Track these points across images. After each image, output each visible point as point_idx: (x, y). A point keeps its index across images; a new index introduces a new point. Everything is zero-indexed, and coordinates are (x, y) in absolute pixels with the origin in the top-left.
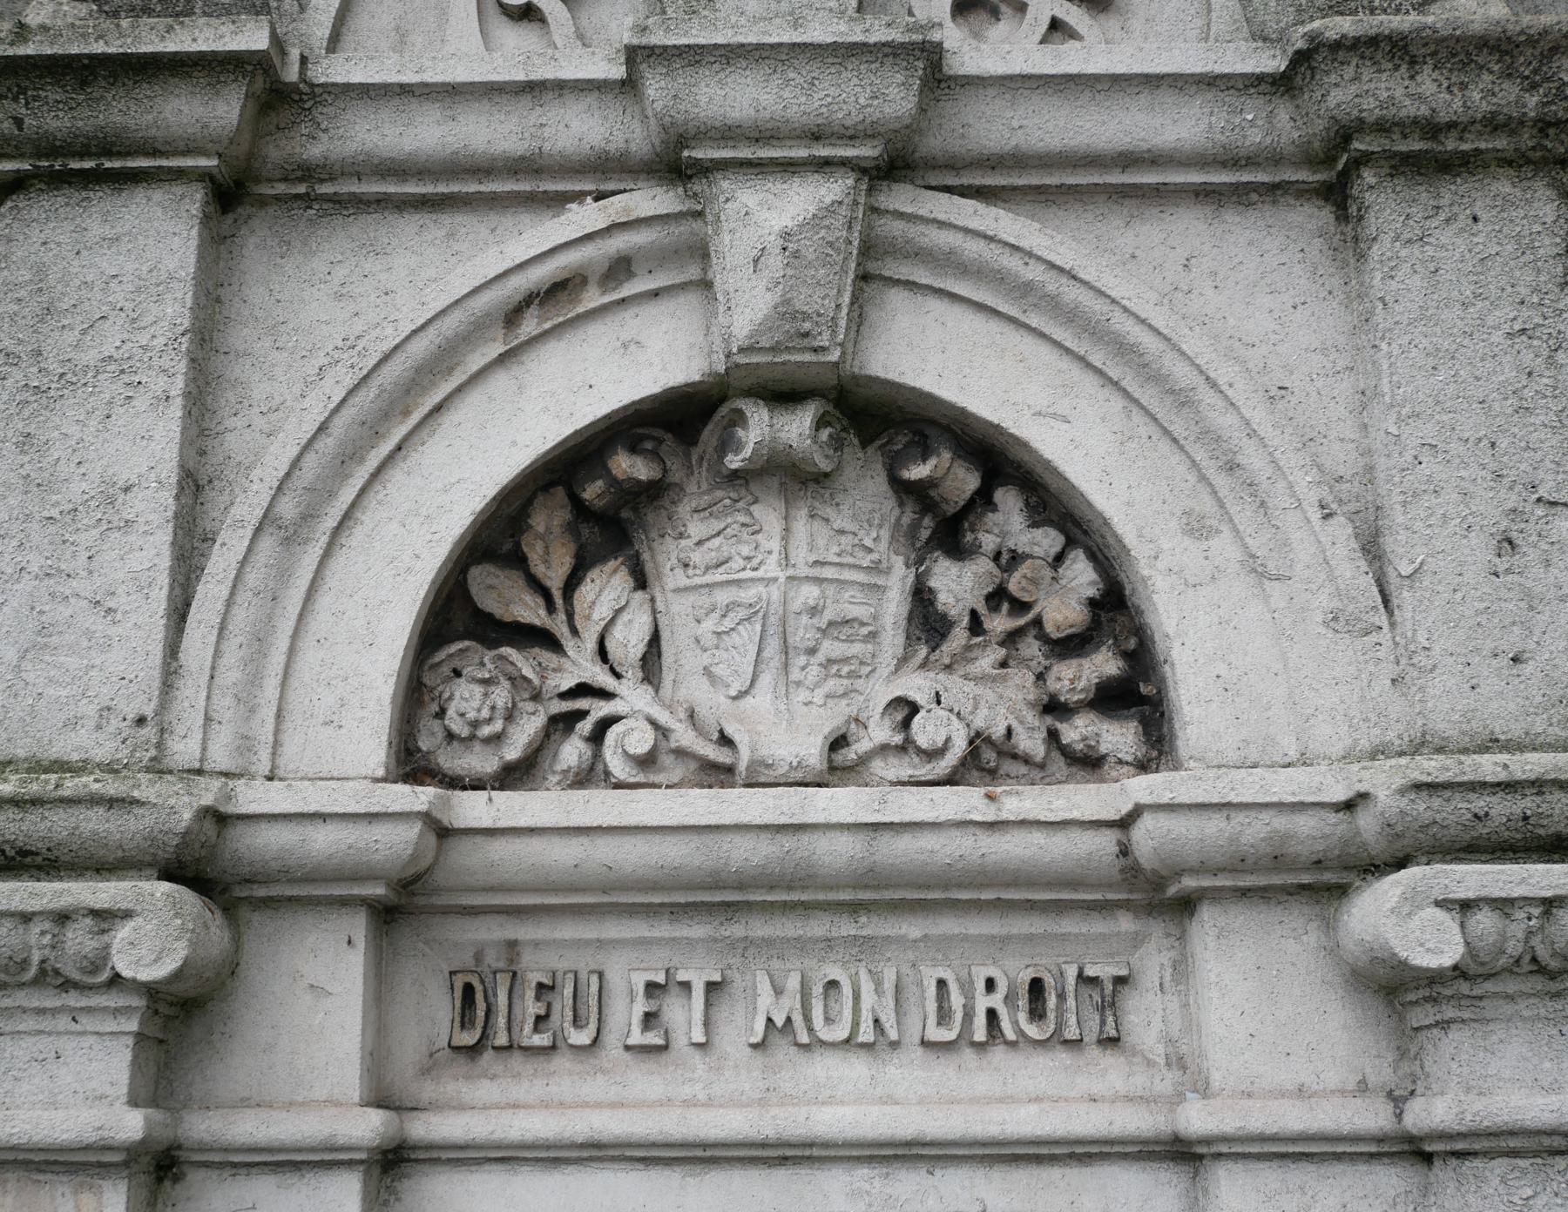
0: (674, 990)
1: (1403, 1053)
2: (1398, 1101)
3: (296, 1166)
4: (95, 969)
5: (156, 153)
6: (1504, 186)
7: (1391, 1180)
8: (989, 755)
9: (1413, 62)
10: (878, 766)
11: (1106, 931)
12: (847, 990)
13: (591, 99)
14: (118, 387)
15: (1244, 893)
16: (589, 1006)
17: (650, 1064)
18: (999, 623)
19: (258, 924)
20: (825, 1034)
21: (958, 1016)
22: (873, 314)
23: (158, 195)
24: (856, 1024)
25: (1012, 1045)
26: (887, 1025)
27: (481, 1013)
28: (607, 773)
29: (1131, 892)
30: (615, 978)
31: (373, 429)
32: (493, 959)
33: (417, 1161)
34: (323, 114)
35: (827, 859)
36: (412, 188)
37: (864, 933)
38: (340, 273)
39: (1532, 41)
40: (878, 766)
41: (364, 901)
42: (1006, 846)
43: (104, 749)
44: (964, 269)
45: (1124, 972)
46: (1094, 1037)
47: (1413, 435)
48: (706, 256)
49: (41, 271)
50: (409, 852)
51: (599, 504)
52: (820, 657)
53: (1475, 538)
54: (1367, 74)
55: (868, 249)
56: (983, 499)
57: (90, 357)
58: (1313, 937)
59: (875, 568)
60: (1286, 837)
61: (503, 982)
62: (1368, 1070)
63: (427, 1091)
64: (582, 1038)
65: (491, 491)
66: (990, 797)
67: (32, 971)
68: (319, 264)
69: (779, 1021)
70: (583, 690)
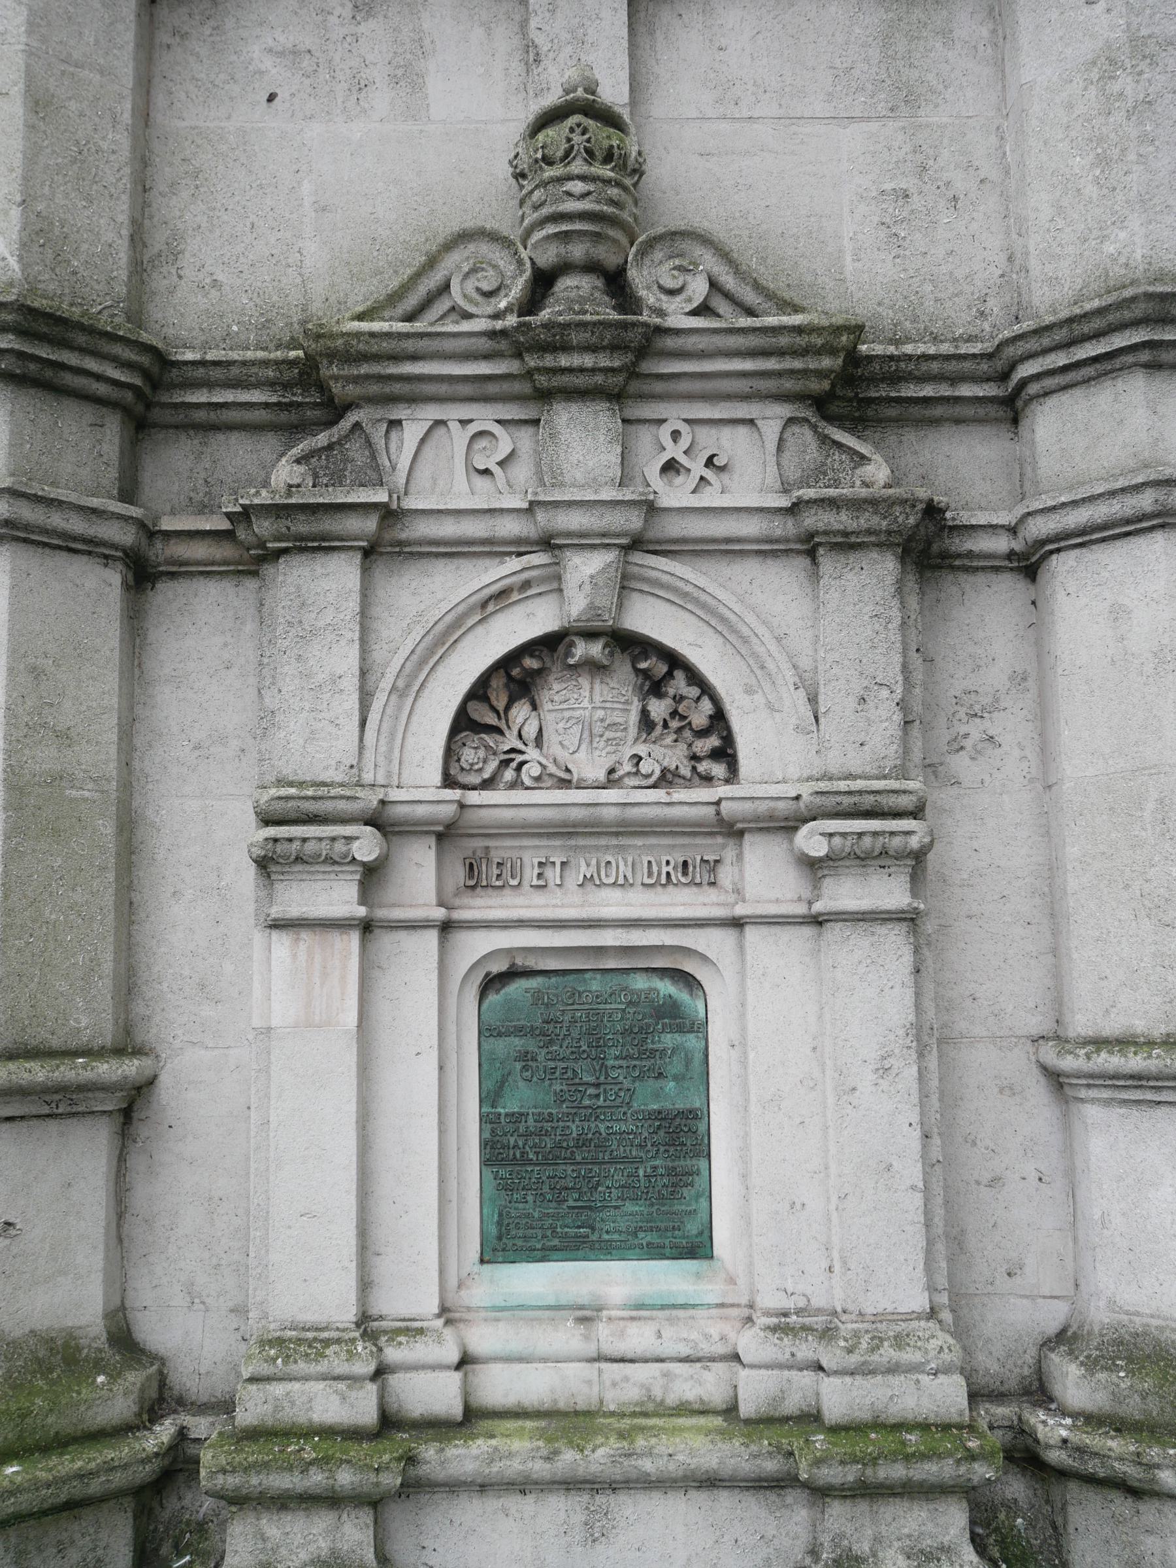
1: (815, 887)
2: (810, 903)
3: (414, 927)
4: (346, 857)
5: (342, 540)
6: (874, 555)
7: (808, 931)
8: (669, 776)
9: (838, 507)
10: (626, 781)
12: (614, 864)
13: (514, 515)
14: (333, 636)
15: (761, 829)
17: (540, 892)
18: (675, 724)
22: (626, 602)
23: (343, 556)
24: (617, 877)
25: (676, 885)
28: (523, 783)
30: (526, 860)
31: (431, 651)
32: (479, 854)
34: (407, 521)
36: (442, 549)
38: (414, 584)
39: (884, 500)
40: (626, 781)
41: (434, 832)
43: (339, 778)
44: (662, 586)
47: (831, 657)
48: (560, 579)
49: (299, 588)
51: (518, 677)
52: (605, 738)
53: (850, 698)
54: (820, 512)
55: (624, 577)
56: (670, 675)
57: (321, 624)
58: (785, 846)
59: (626, 702)
60: (774, 809)
61: (484, 862)
63: (457, 902)
64: (515, 882)
65: (478, 675)
66: (668, 793)
67: (293, 857)
68: (405, 580)
70: (513, 750)
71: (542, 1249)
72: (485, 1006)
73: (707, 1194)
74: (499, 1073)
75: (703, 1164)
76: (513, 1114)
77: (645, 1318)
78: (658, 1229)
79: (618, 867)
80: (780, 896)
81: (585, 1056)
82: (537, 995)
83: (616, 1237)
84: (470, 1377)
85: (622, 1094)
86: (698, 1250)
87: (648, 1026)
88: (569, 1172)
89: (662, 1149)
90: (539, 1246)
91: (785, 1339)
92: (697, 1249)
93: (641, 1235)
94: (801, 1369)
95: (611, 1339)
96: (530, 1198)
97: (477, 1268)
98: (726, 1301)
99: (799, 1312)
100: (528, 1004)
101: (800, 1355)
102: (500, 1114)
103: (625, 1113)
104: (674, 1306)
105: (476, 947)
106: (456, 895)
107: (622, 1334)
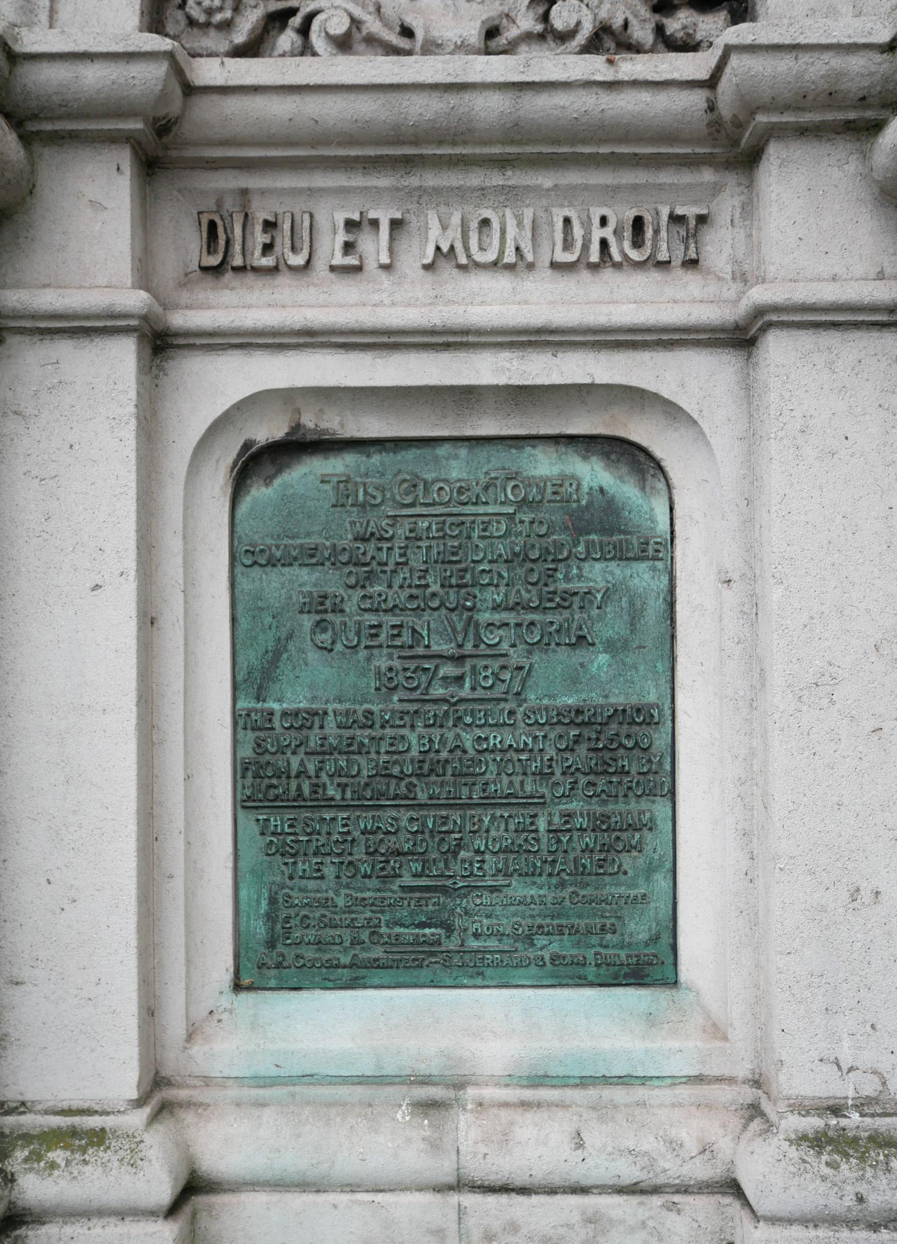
0: (366, 228)
11: (693, 181)
16: (305, 236)
19: (48, 155)
20: (479, 257)
21: (579, 244)
24: (502, 252)
26: (525, 251)
27: (222, 242)
29: (714, 147)
30: (322, 220)
32: (229, 204)
33: (179, 347)
35: (483, 115)
37: (510, 183)
42: (620, 103)
45: (704, 212)
46: (679, 262)
50: (160, 87)
58: (853, 166)
60: (840, 75)
62: (886, 264)
64: (298, 260)
66: (610, 62)
69: (445, 248)
71: (351, 966)
72: (244, 507)
73: (668, 865)
74: (271, 635)
75: (661, 809)
76: (296, 713)
77: (550, 1105)
78: (574, 930)
79: (503, 232)
80: (838, 270)
81: (435, 603)
82: (344, 488)
83: (492, 943)
84: (204, 1221)
85: (507, 676)
86: (648, 969)
87: (559, 546)
88: (404, 823)
89: (583, 780)
90: (345, 960)
91: (844, 1167)
92: (650, 966)
93: (541, 941)
94: (874, 1227)
95: (483, 1149)
96: (329, 871)
97: (228, 999)
98: (707, 1071)
99: (863, 1105)
100: (327, 505)
101: (874, 1201)
102: (271, 713)
103: (511, 713)
104: (606, 1080)
105: (217, 385)
106: (182, 285)
107: (505, 1138)
